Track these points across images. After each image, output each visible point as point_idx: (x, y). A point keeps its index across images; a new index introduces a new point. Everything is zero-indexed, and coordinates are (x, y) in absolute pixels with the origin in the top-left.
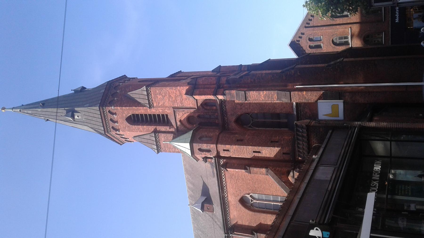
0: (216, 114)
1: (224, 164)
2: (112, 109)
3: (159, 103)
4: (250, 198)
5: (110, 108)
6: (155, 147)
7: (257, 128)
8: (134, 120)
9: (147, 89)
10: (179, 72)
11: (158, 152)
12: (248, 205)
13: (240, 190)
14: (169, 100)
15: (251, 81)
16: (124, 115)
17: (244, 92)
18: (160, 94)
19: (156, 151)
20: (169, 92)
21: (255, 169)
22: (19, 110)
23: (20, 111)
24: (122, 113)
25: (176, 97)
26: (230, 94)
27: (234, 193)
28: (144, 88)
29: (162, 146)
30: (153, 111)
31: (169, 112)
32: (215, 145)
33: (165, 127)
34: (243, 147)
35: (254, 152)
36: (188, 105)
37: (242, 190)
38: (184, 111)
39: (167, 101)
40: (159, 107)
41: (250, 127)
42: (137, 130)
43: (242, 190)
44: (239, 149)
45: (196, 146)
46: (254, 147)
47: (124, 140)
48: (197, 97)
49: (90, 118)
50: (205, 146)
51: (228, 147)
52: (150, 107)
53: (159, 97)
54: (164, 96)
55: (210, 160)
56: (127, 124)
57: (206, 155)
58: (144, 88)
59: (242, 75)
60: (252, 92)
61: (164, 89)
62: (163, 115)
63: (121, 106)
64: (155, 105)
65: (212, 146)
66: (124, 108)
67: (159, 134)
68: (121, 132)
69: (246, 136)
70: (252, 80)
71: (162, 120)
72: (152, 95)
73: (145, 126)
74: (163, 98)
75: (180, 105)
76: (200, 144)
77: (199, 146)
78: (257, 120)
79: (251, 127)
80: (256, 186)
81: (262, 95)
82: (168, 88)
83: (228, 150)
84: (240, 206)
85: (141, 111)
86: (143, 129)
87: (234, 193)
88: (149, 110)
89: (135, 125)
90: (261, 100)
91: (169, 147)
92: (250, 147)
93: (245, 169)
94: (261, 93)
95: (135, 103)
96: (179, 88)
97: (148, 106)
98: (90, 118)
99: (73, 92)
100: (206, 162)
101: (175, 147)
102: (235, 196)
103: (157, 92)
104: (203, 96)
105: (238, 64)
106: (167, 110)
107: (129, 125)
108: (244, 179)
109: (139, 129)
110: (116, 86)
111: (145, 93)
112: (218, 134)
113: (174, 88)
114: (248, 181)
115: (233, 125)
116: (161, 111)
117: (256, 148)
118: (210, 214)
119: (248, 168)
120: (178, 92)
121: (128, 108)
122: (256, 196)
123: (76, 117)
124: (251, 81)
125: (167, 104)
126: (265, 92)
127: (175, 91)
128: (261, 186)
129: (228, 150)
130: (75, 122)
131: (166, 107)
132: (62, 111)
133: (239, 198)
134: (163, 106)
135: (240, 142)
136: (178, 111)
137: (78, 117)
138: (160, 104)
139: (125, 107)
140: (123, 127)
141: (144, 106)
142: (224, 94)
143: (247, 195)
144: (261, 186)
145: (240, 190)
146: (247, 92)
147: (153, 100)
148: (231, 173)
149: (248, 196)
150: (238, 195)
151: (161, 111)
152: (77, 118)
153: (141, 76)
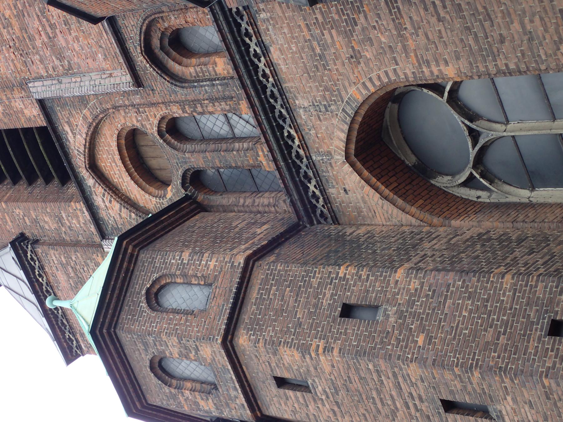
41: (470, 182)
69: (400, 274)
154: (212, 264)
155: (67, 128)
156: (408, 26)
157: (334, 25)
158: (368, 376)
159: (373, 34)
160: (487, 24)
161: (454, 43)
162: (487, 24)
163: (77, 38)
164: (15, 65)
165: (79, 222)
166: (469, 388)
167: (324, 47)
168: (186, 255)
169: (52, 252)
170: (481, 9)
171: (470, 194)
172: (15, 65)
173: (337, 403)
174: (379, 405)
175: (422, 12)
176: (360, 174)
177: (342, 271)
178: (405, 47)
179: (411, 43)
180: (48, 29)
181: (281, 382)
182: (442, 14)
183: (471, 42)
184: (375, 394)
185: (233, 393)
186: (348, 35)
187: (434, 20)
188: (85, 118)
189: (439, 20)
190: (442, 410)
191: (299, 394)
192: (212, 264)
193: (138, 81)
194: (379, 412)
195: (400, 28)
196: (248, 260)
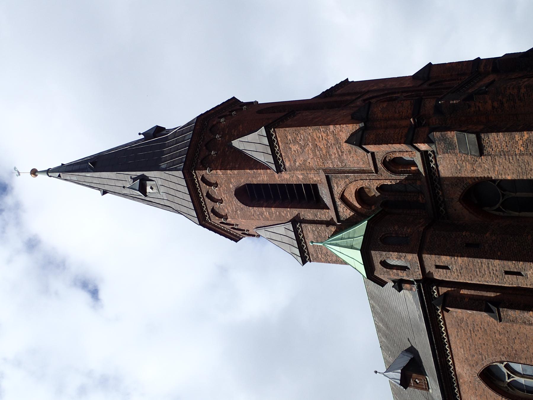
0: (418, 183)
1: (436, 299)
2: (206, 173)
3: (295, 161)
4: (505, 371)
5: (204, 172)
6: (297, 251)
7: (517, 214)
8: (251, 195)
9: (268, 132)
10: (342, 82)
11: (304, 262)
12: (501, 384)
13: (481, 354)
14: (315, 155)
15: (493, 107)
16: (231, 186)
17: (474, 136)
18: (295, 141)
19: (300, 259)
20: (312, 137)
21: (512, 313)
22: (58, 174)
23: (59, 176)
24: (226, 182)
25: (328, 148)
26: (444, 139)
27: (467, 359)
28: (262, 131)
29: (311, 250)
30: (285, 178)
31: (318, 178)
32: (416, 256)
33: (312, 211)
34: (479, 260)
35: (507, 273)
36: (356, 165)
37: (485, 354)
38: (347, 177)
39: (311, 156)
40: (297, 170)
41: (498, 210)
42: (258, 215)
43: (485, 354)
44: (471, 266)
45: (377, 256)
46: (506, 262)
47: (240, 232)
48: (371, 148)
49: (172, 192)
50: (394, 259)
51: (445, 260)
52: (279, 171)
53: (295, 148)
54: (305, 146)
55: (408, 286)
56: (239, 204)
57: (398, 275)
58: (262, 131)
59: (470, 91)
60: (494, 135)
61: (302, 132)
62: (307, 186)
63: (224, 167)
64: (287, 164)
65: (413, 258)
66: (229, 171)
67: (303, 225)
68: (229, 220)
69: (488, 235)
70: (496, 104)
71: (303, 196)
72: (280, 144)
73: (273, 209)
74: (303, 151)
75: (338, 165)
76: (384, 253)
77: (381, 255)
78: (513, 194)
79: (502, 211)
80: (517, 346)
81: (521, 142)
82: (310, 130)
83: (446, 268)
84: (483, 385)
85: (262, 177)
86: (271, 214)
87: (467, 359)
88: (276, 175)
89: (253, 206)
90: (517, 152)
91: (324, 251)
92: (497, 262)
93: (488, 310)
94: (517, 136)
95: (245, 161)
96: (331, 127)
97: (274, 167)
98: (172, 192)
99: (142, 137)
100: (400, 289)
101: (333, 254)
102: (470, 365)
103: (289, 137)
104: (385, 146)
105: (472, 57)
106: (312, 176)
107: (242, 206)
108: (488, 332)
109: (262, 214)
110: (214, 126)
111: (266, 141)
112: (421, 229)
113: (322, 128)
114: (497, 336)
115: (458, 208)
116: (301, 177)
117: (511, 265)
118: (424, 392)
119: (494, 309)
120: (331, 137)
121: (236, 172)
122: (518, 367)
123: (149, 190)
124: (493, 107)
125: (312, 162)
126: (526, 135)
127: (324, 135)
128: (528, 347)
129: (446, 268)
130: (147, 199)
131: (311, 169)
132: (126, 178)
133: (479, 368)
134: (304, 168)
135: (473, 250)
136: (336, 178)
137: (152, 188)
138: (297, 164)
139: (231, 169)
140: (232, 211)
141: (268, 168)
142: (430, 141)
143: (498, 364)
144: (528, 347)
145: (481, 354)
146: (482, 136)
147: (283, 154)
148: (454, 318)
149: (502, 366)
150: (477, 363)
151: (301, 177)
152: (151, 191)
153: (264, 97)
154: (409, 230)
155: (335, 185)
156: (497, 164)
157: (468, 161)
158: (477, 265)
159: (483, 165)
160: (527, 166)
161: (513, 170)
162: (527, 166)
163: (353, 157)
164: (318, 163)
165: (325, 216)
166: (517, 267)
167: (461, 167)
168: (396, 228)
169: (309, 226)
170: (526, 161)
171: (497, 213)
172: (318, 163)
173: (460, 273)
174: (478, 273)
175: (504, 160)
176: (463, 205)
177: (464, 234)
178: (494, 169)
179: (497, 169)
180: (340, 153)
181: (437, 267)
182: (511, 161)
183: (520, 170)
184: (478, 270)
185: (416, 270)
186: (472, 164)
187: (507, 163)
188: (345, 182)
189: (510, 163)
190: (504, 274)
191: (444, 270)
192: (409, 230)
193: (377, 171)
194: (477, 275)
195: (494, 164)
196: (424, 230)
